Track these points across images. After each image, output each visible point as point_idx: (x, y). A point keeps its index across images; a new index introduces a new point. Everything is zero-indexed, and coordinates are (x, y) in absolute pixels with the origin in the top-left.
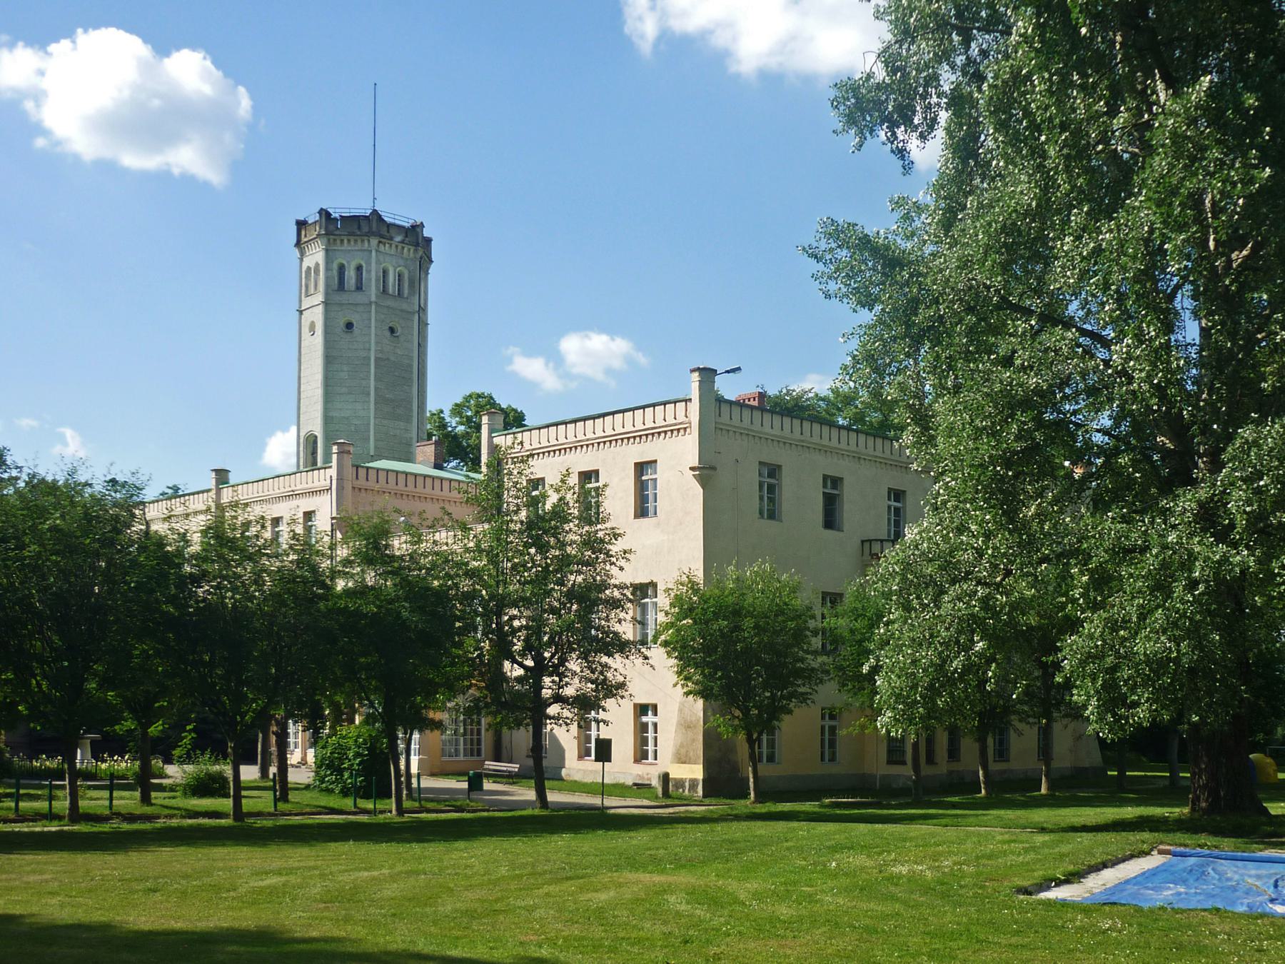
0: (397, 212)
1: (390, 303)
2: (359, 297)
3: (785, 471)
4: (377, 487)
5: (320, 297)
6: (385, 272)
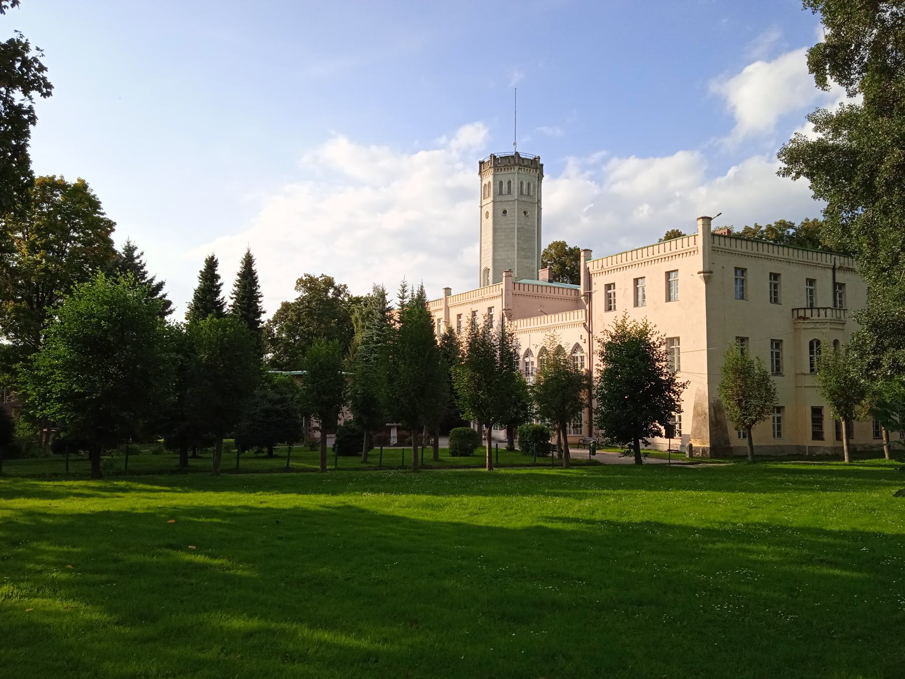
0: (527, 153)
1: (523, 199)
2: (509, 198)
3: (782, 277)
4: (524, 293)
5: (491, 199)
6: (522, 183)
